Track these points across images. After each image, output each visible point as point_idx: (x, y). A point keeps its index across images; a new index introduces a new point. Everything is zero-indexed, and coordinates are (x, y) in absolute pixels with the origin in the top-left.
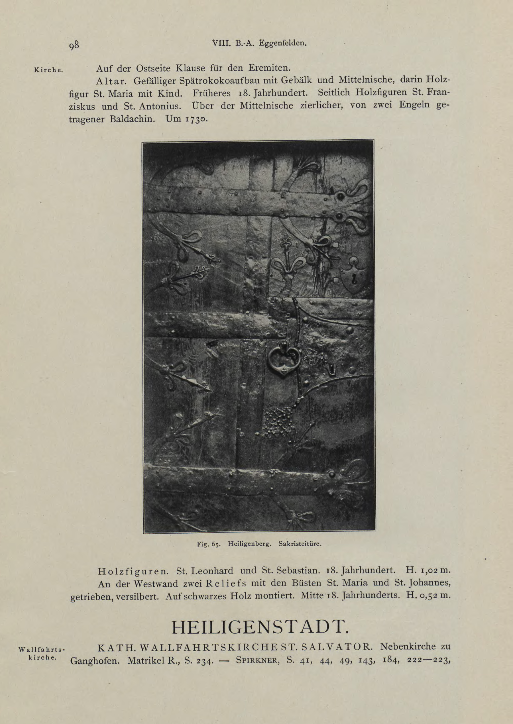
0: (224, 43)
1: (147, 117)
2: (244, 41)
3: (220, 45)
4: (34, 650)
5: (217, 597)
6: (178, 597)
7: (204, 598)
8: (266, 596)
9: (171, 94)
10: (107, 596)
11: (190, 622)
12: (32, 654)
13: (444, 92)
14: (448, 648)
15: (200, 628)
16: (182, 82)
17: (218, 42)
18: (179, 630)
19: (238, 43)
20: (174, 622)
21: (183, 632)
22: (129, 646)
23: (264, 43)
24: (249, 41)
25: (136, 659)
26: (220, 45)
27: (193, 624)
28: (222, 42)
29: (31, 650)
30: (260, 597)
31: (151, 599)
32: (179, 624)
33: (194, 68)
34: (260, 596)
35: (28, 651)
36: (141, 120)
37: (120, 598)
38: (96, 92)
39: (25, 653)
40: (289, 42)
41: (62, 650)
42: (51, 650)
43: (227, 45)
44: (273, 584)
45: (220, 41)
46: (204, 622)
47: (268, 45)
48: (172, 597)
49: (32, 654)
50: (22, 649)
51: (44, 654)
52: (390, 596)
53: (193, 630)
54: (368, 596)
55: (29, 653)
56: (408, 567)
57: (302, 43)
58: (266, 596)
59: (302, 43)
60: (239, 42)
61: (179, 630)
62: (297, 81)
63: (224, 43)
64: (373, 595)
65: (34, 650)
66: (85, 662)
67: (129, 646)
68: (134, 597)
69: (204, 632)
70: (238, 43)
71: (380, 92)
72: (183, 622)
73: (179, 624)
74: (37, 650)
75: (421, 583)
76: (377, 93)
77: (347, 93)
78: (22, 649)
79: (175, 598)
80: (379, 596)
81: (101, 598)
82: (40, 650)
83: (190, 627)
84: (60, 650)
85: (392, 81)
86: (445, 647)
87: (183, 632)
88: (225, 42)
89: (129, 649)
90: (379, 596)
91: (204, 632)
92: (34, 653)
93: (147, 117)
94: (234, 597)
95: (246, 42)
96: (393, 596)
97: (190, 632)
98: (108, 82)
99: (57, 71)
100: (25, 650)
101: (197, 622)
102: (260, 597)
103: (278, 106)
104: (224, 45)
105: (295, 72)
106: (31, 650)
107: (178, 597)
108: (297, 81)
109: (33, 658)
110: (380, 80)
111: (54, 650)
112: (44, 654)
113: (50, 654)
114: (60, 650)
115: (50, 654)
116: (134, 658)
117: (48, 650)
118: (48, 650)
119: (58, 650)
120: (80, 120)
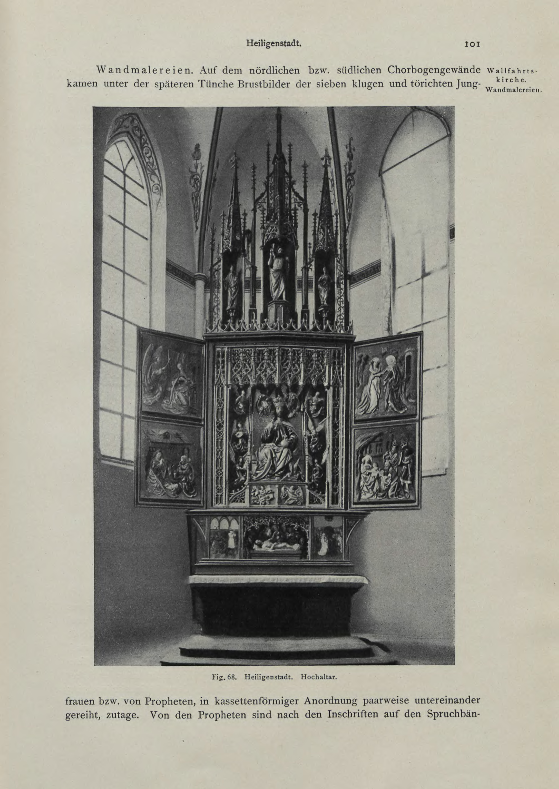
4: (504, 71)
5: (315, 71)
6: (213, 70)
7: (457, 72)
8: (321, 702)
9: (263, 715)
10: (318, 714)
12: (500, 76)
13: (474, 714)
14: (280, 715)
16: (430, 715)
30: (84, 85)
31: (437, 703)
33: (392, 714)
34: (84, 84)
35: (498, 72)
36: (350, 715)
37: (128, 703)
42: (522, 72)
44: (308, 715)
48: (207, 71)
49: (500, 76)
50: (490, 70)
51: (512, 76)
54: (343, 702)
55: (497, 75)
58: (321, 702)
62: (463, 714)
64: (398, 84)
65: (504, 71)
68: (257, 715)
74: (507, 71)
75: (224, 715)
77: (296, 715)
78: (490, 70)
79: (210, 71)
80: (468, 701)
81: (228, 716)
82: (511, 71)
84: (532, 71)
85: (136, 716)
86: (111, 715)
90: (472, 70)
94: (304, 678)
100: (495, 71)
102: (84, 85)
103: (341, 715)
106: (500, 71)
107: (213, 70)
108: (463, 714)
109: (501, 80)
110: (345, 715)
111: (526, 72)
112: (512, 76)
113: (520, 76)
114: (532, 71)
115: (520, 76)
118: (519, 71)
119: (530, 72)
120: (125, 716)
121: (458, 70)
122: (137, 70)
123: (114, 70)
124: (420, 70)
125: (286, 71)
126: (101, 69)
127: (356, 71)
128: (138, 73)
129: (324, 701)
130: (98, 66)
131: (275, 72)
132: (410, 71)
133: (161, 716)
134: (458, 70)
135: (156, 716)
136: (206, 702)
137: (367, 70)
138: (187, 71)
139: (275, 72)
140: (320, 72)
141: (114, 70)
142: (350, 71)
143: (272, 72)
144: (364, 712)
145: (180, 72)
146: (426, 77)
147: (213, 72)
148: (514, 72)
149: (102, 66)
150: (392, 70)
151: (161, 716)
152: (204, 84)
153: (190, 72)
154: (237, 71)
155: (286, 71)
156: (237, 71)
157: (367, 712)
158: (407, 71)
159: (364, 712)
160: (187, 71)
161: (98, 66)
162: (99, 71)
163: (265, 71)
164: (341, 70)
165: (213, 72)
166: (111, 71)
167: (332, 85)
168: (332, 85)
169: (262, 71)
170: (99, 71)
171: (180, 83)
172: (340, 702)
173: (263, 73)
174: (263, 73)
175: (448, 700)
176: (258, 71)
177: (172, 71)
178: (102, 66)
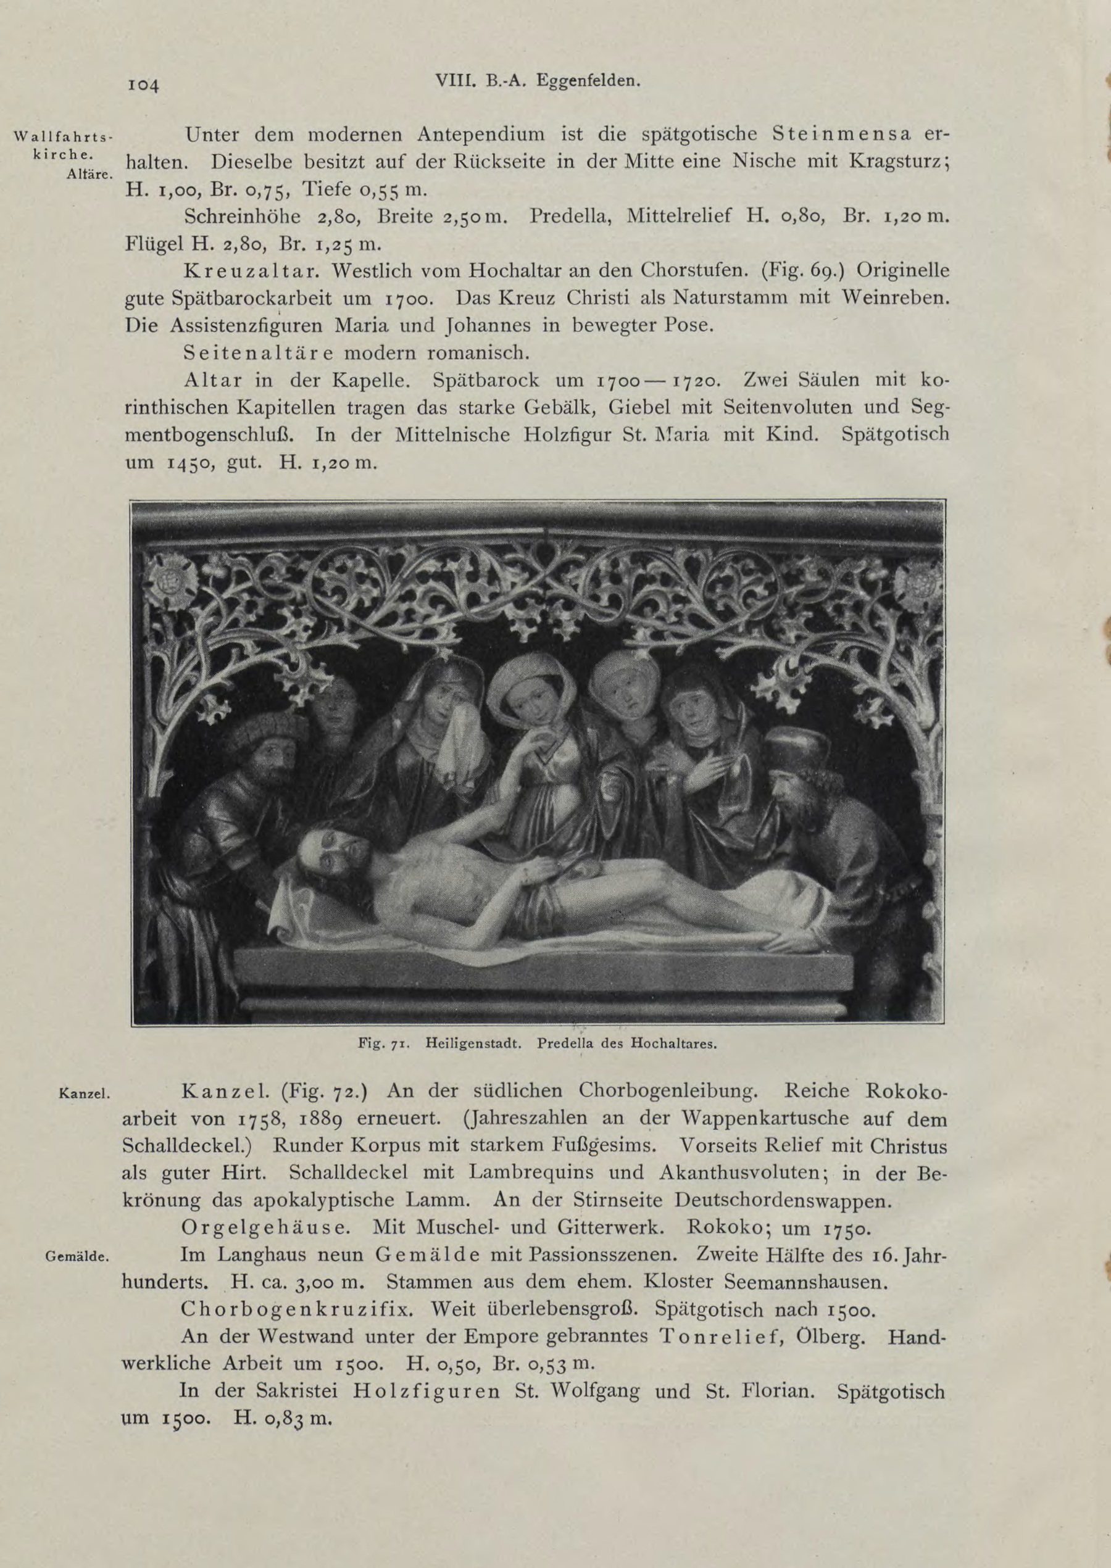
0: (460, 80)
1: (572, 1168)
2: (504, 76)
7: (828, 1205)
12: (40, 146)
19: (492, 79)
23: (547, 79)
24: (514, 76)
25: (352, 322)
26: (452, 85)
29: (40, 137)
35: (35, 138)
38: (392, 1277)
39: (28, 144)
40: (601, 77)
41: (107, 138)
42: (83, 138)
50: (20, 136)
52: (186, 1284)
57: (630, 82)
59: (630, 82)
60: (492, 77)
63: (460, 80)
66: (247, 1256)
70: (492, 79)
71: (263, 326)
74: (54, 138)
76: (257, 327)
78: (20, 136)
82: (61, 138)
84: (103, 139)
92: (47, 144)
93: (572, 1168)
95: (509, 78)
96: (193, 1284)
98: (283, 354)
100: (28, 137)
104: (460, 75)
106: (40, 137)
109: (42, 156)
111: (91, 139)
113: (78, 148)
114: (103, 139)
115: (78, 148)
116: (349, 319)
119: (98, 138)
121: (320, 1338)
122: (200, 1255)
123: (214, 1093)
124: (644, 1092)
125: (535, 1091)
127: (513, 1091)
129: (708, 1146)
132: (140, 1121)
133: (701, 1147)
134: (320, 1338)
135: (693, 1147)
136: (855, 1174)
137: (535, 1092)
141: (214, 1093)
142: (500, 1092)
144: (807, 1252)
145: (250, 1095)
150: (588, 1090)
151: (701, 1147)
154: (936, 1121)
156: (936, 1121)
157: (815, 1252)
158: (773, 1393)
159: (807, 1252)
162: (264, 1340)
164: (482, 1091)
166: (208, 1094)
170: (264, 1340)
175: (699, 162)
177: (811, 136)
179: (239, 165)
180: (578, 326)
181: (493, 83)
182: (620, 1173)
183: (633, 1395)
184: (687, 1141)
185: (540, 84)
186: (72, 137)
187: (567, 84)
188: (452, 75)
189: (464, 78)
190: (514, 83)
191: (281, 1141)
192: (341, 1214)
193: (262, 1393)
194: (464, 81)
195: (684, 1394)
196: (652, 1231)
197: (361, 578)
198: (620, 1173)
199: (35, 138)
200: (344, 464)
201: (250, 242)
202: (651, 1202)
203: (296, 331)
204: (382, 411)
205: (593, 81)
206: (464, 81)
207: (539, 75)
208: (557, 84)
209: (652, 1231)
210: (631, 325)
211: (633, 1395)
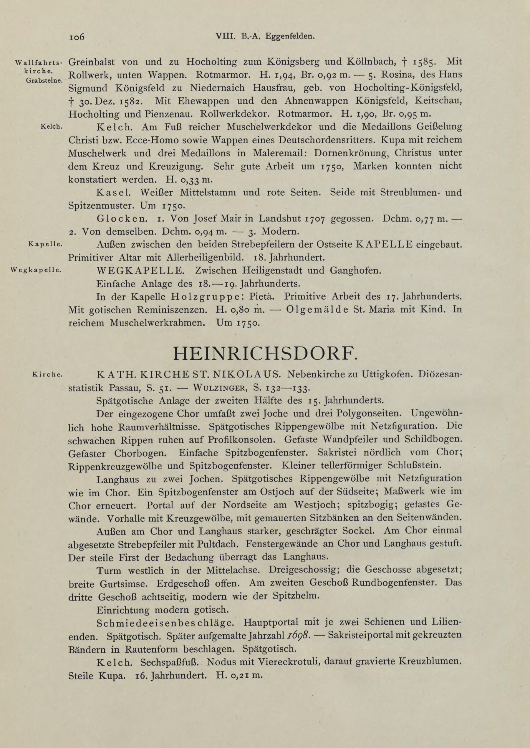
0: (229, 36)
2: (250, 34)
3: (224, 38)
4: (31, 63)
11: (192, 348)
12: (28, 67)
15: (203, 354)
17: (222, 35)
18: (180, 357)
19: (244, 36)
20: (176, 348)
21: (185, 359)
22: (129, 373)
23: (271, 36)
26: (224, 38)
27: (195, 350)
28: (226, 35)
29: (28, 63)
32: (180, 350)
35: (25, 64)
41: (59, 63)
42: (48, 63)
43: (232, 38)
45: (224, 33)
46: (207, 348)
47: (276, 38)
50: (18, 62)
53: (196, 356)
56: (343, 111)
57: (310, 36)
60: (244, 34)
61: (180, 357)
63: (229, 36)
65: (31, 63)
67: (129, 373)
69: (207, 359)
70: (244, 36)
72: (185, 348)
73: (180, 350)
74: (34, 63)
78: (18, 62)
79: (107, 246)
82: (38, 63)
83: (193, 353)
84: (58, 63)
87: (185, 359)
88: (230, 35)
89: (130, 376)
91: (207, 359)
92: (31, 66)
95: (252, 35)
97: (193, 359)
99: (46, 71)
100: (22, 63)
101: (200, 348)
104: (228, 33)
105: (365, 358)
106: (28, 63)
109: (29, 72)
111: (52, 64)
113: (46, 68)
114: (58, 63)
115: (46, 68)
117: (45, 63)
118: (45, 63)
119: (55, 63)
126: (256, 676)
128: (335, 507)
129: (124, 493)
130: (213, 137)
131: (388, 454)
138: (142, 219)
139: (388, 454)
140: (345, 624)
143: (385, 454)
146: (211, 264)
147: (349, 663)
148: (40, 64)
149: (216, 137)
152: (103, 571)
153: (154, 181)
155: (258, 427)
157: (277, 399)
160: (142, 219)
161: (213, 137)
162: (297, 506)
163: (240, 506)
165: (349, 663)
167: (139, 545)
168: (139, 545)
169: (375, 453)
170: (297, 506)
171: (312, 61)
172: (90, 90)
173: (76, 587)
174: (76, 587)
176: (372, 453)
178: (216, 137)
179: (295, 402)
180: (201, 245)
181: (245, 37)
182: (249, 193)
183: (293, 192)
184: (111, 517)
185: (267, 38)
186: (43, 63)
187: (280, 38)
188: (224, 33)
189: (230, 35)
190: (255, 38)
191: (124, 439)
192: (266, 460)
193: (321, 454)
194: (230, 36)
195: (307, 414)
196: (124, 155)
197: (229, 298)
198: (313, 271)
199: (25, 64)
200: (247, 310)
201: (244, 309)
202: (369, 492)
203: (165, 156)
204: (312, 428)
205: (292, 36)
206: (230, 36)
207: (267, 33)
208: (276, 38)
209: (124, 155)
210: (325, 531)
211: (293, 192)
